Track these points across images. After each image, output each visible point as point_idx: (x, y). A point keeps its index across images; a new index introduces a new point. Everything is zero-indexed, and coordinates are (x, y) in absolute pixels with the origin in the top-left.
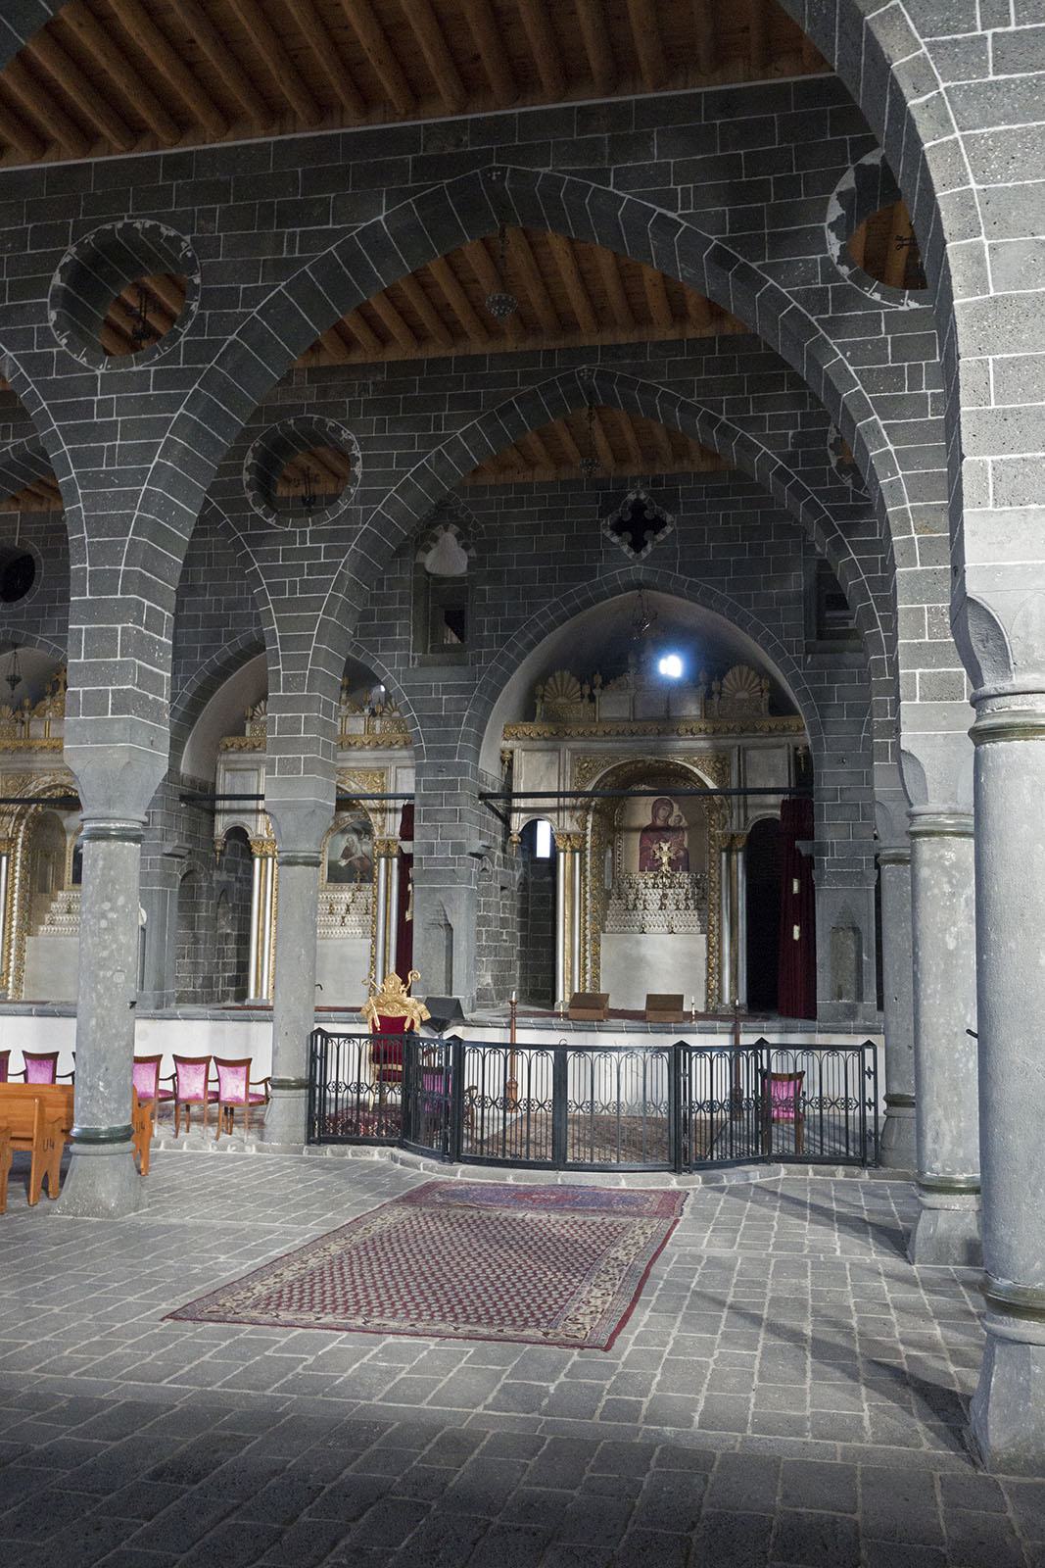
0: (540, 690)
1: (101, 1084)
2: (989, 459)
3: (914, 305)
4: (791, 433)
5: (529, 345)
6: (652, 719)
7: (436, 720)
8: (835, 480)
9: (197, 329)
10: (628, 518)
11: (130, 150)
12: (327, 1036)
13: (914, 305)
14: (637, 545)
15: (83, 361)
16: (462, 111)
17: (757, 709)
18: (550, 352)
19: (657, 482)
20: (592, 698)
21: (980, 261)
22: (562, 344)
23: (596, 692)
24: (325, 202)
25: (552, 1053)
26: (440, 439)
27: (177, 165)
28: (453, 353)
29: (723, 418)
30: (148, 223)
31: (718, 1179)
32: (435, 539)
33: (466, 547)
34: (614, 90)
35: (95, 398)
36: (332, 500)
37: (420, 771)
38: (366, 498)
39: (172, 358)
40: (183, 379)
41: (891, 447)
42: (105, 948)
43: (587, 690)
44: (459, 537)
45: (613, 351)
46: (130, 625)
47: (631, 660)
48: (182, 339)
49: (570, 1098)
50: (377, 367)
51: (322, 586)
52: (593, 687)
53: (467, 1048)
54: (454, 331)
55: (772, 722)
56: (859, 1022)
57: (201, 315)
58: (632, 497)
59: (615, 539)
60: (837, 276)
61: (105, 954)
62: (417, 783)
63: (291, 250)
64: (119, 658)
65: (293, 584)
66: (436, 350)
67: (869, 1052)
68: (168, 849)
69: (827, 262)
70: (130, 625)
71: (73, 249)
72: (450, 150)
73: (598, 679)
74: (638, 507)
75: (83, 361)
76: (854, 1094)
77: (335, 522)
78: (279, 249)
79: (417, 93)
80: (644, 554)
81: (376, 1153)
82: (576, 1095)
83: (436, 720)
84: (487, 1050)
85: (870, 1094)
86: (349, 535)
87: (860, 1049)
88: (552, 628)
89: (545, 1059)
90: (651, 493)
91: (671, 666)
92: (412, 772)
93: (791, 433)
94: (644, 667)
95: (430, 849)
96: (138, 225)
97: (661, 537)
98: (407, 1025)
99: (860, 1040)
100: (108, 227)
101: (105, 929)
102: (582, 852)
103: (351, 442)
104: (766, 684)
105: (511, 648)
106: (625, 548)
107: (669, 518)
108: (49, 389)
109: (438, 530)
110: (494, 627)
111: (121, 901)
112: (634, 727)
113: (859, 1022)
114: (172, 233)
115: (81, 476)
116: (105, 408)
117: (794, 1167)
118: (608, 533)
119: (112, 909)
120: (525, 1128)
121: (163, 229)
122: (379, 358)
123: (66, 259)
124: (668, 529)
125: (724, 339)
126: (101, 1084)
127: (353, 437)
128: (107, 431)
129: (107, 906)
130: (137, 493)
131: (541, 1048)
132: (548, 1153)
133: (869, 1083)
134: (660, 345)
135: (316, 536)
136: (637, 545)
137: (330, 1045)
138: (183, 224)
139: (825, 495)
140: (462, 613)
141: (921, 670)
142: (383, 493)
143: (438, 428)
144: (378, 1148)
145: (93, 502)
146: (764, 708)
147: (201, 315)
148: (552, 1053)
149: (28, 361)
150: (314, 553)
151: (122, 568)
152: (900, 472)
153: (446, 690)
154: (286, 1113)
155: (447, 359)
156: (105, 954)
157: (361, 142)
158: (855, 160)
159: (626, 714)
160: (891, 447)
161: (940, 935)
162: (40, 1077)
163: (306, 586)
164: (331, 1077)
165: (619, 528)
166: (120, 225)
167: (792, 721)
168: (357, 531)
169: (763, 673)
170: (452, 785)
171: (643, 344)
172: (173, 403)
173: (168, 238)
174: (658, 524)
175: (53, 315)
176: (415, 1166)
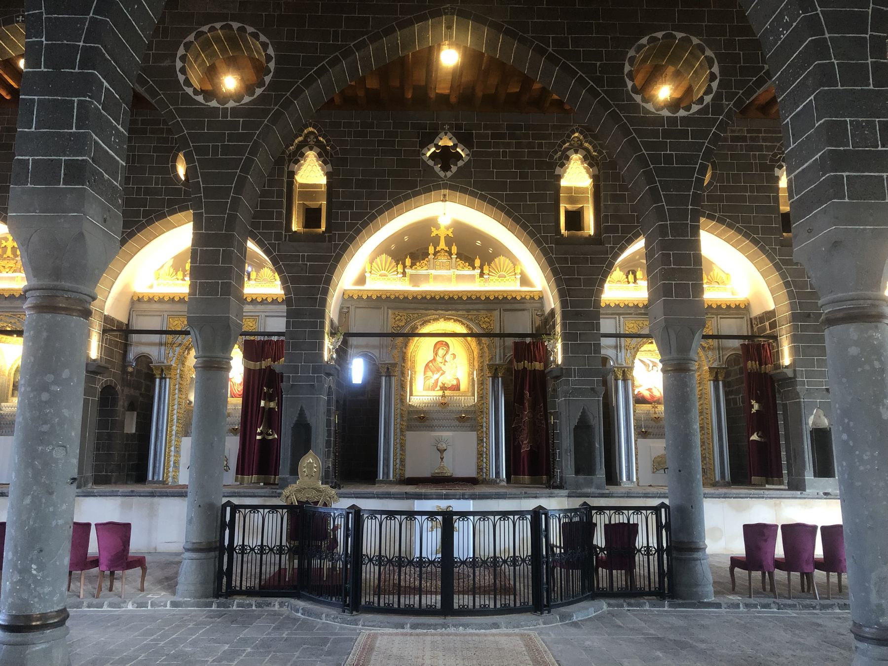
1: (34, 566)
4: (598, 63)
12: (235, 508)
25: (440, 518)
29: (550, 50)
31: (570, 616)
35: (43, 39)
42: (45, 423)
43: (400, 269)
46: (87, 99)
49: (530, 567)
52: (405, 267)
53: (365, 516)
61: (45, 428)
64: (74, 130)
65: (215, 148)
70: (87, 99)
73: (408, 262)
81: (277, 604)
82: (461, 552)
84: (384, 516)
89: (374, 521)
92: (285, 319)
93: (598, 63)
101: (46, 402)
111: (66, 374)
117: (612, 601)
119: (55, 383)
120: (396, 577)
126: (34, 566)
129: (50, 378)
131: (431, 515)
132: (436, 600)
136: (446, 168)
137: (237, 515)
141: (847, 174)
143: (336, 38)
144: (279, 599)
148: (440, 518)
151: (81, 44)
152: (819, 9)
154: (189, 573)
156: (45, 428)
161: (874, 407)
163: (226, 150)
164: (238, 541)
168: (269, 110)
176: (319, 616)
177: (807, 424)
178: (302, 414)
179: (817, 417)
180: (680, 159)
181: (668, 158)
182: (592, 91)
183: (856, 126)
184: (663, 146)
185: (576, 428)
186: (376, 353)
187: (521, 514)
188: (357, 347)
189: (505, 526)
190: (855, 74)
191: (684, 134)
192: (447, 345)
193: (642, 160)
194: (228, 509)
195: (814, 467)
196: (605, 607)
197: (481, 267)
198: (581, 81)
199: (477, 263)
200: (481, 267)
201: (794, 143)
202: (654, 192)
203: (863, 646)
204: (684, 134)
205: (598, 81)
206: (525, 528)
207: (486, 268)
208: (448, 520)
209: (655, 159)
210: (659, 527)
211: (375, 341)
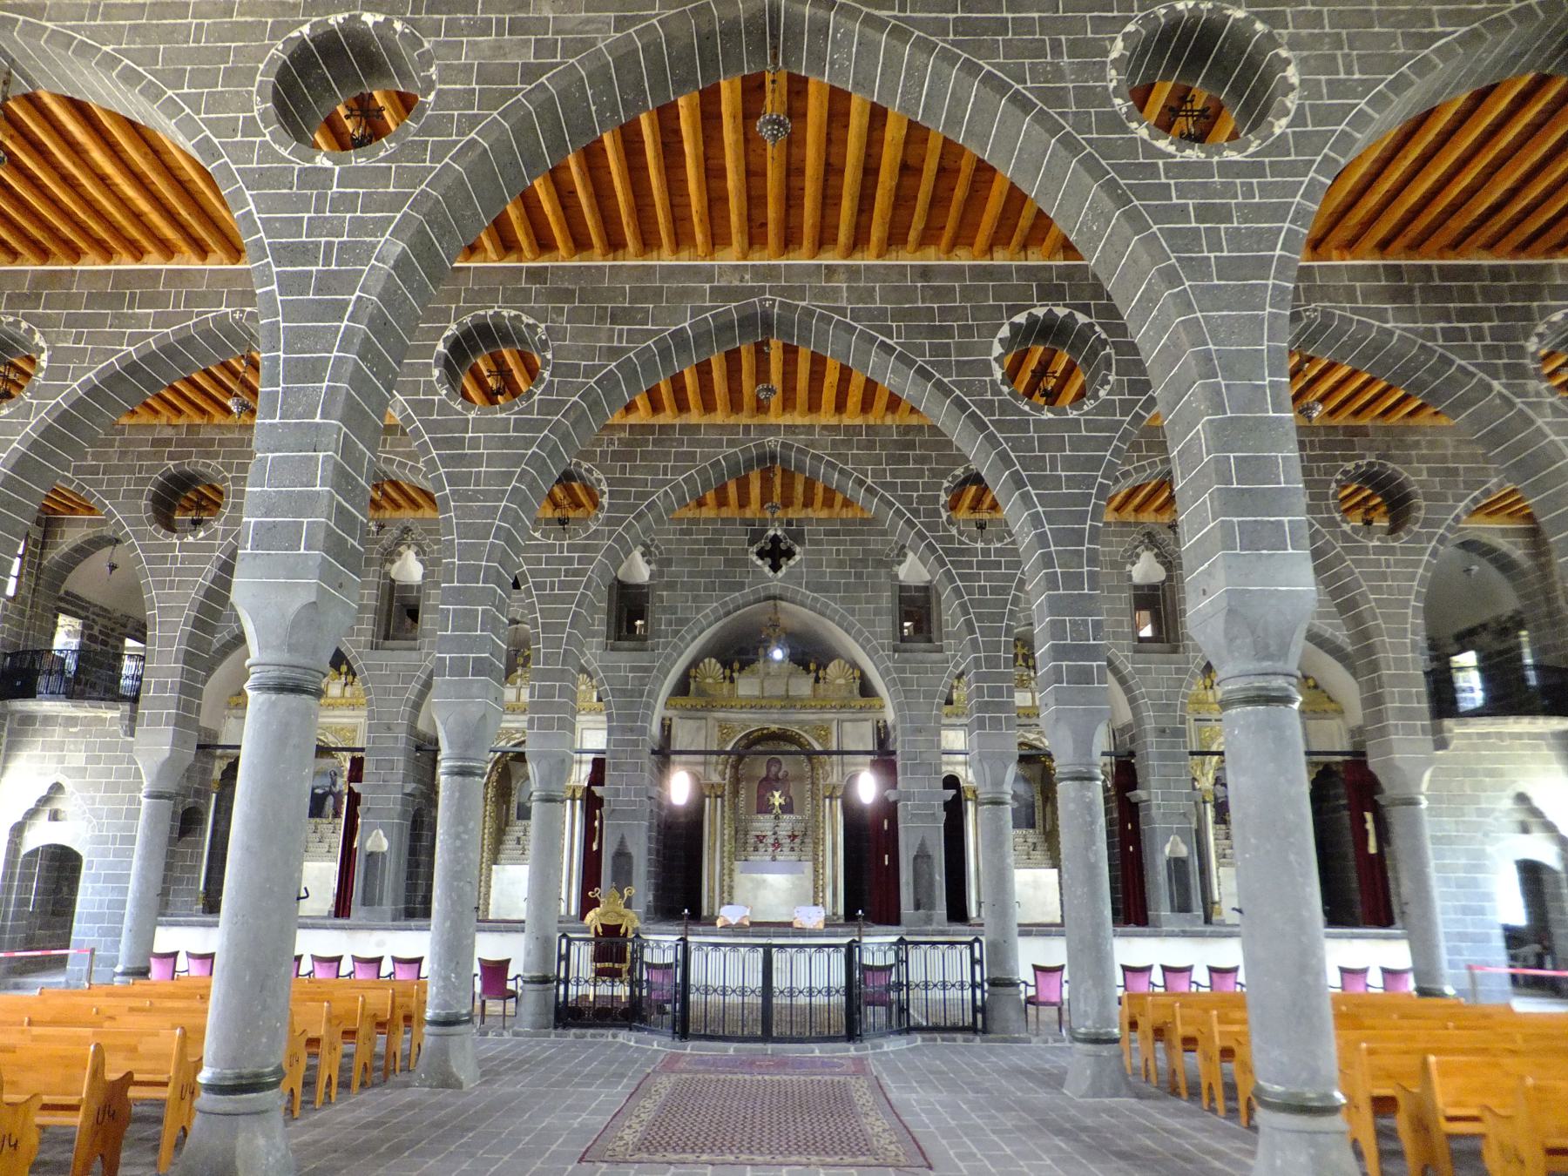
0: (693, 672)
2: (1235, 519)
3: (1051, 416)
5: (732, 420)
6: (778, 697)
7: (624, 692)
8: (945, 530)
9: (549, 389)
10: (768, 547)
11: (500, 260)
13: (1051, 416)
14: (775, 567)
15: (459, 408)
16: (745, 258)
17: (851, 692)
18: (747, 428)
19: (789, 523)
20: (732, 680)
21: (1219, 393)
22: (755, 421)
23: (735, 675)
24: (646, 311)
26: (665, 483)
27: (536, 275)
28: (677, 421)
30: (513, 313)
31: (881, 1046)
32: (400, 554)
33: (649, 562)
34: (848, 255)
36: (582, 521)
37: (610, 731)
38: (609, 521)
39: (529, 410)
40: (536, 426)
41: (1040, 509)
44: (643, 555)
45: (791, 429)
47: (761, 651)
48: (536, 397)
50: (622, 427)
51: (575, 586)
54: (682, 406)
55: (863, 702)
56: (934, 927)
57: (552, 382)
58: (771, 533)
59: (759, 562)
60: (1000, 393)
62: (608, 741)
63: (620, 341)
66: (667, 417)
67: (977, 945)
68: (408, 790)
69: (993, 382)
71: (453, 326)
72: (736, 283)
73: (736, 666)
74: (775, 539)
75: (459, 408)
76: (967, 978)
77: (587, 538)
78: (611, 339)
79: (717, 239)
80: (780, 574)
83: (624, 692)
85: (978, 979)
86: (596, 549)
87: (971, 945)
88: (710, 625)
90: (785, 531)
91: (778, 654)
92: (605, 733)
94: (768, 659)
95: (617, 793)
96: (505, 313)
97: (792, 563)
98: (622, 930)
99: (970, 939)
100: (482, 313)
102: (722, 796)
103: (599, 481)
104: (857, 673)
105: (682, 639)
106: (767, 569)
107: (798, 549)
108: (430, 426)
109: (402, 549)
110: (670, 623)
112: (764, 703)
113: (934, 927)
114: (531, 321)
115: (453, 492)
116: (474, 443)
117: (927, 1036)
118: (755, 558)
121: (524, 318)
122: (623, 421)
123: (448, 333)
124: (797, 558)
125: (868, 427)
127: (601, 476)
128: (476, 460)
129: (461, 829)
130: (497, 508)
133: (978, 968)
134: (825, 427)
135: (571, 548)
136: (775, 567)
138: (540, 316)
139: (940, 540)
140: (417, 612)
142: (624, 519)
145: (463, 512)
146: (856, 691)
147: (552, 382)
149: (416, 405)
150: (570, 561)
153: (633, 669)
155: (673, 426)
157: (670, 272)
158: (1009, 318)
159: (757, 693)
160: (1040, 509)
162: (404, 974)
165: (761, 554)
166: (491, 312)
167: (875, 701)
169: (854, 665)
170: (635, 743)
171: (812, 427)
172: (528, 443)
173: (528, 325)
174: (789, 554)
175: (436, 372)
177: (1163, 852)
178: (622, 842)
179: (1174, 845)
180: (994, 590)
181: (982, 590)
182: (909, 522)
183: (1073, 623)
184: (976, 577)
185: (915, 858)
186: (701, 769)
187: (836, 946)
188: (680, 763)
189: (820, 959)
190: (1073, 580)
191: (998, 565)
192: (779, 762)
193: (956, 590)
194: (564, 941)
195: (1172, 901)
196: (919, 1042)
197: (817, 671)
198: (898, 513)
199: (812, 666)
200: (817, 671)
201: (1204, 502)
202: (969, 623)
203: (1079, 1045)
204: (998, 565)
205: (915, 512)
206: (839, 959)
207: (821, 673)
208: (343, 696)
209: (970, 591)
210: (974, 962)
211: (700, 758)
